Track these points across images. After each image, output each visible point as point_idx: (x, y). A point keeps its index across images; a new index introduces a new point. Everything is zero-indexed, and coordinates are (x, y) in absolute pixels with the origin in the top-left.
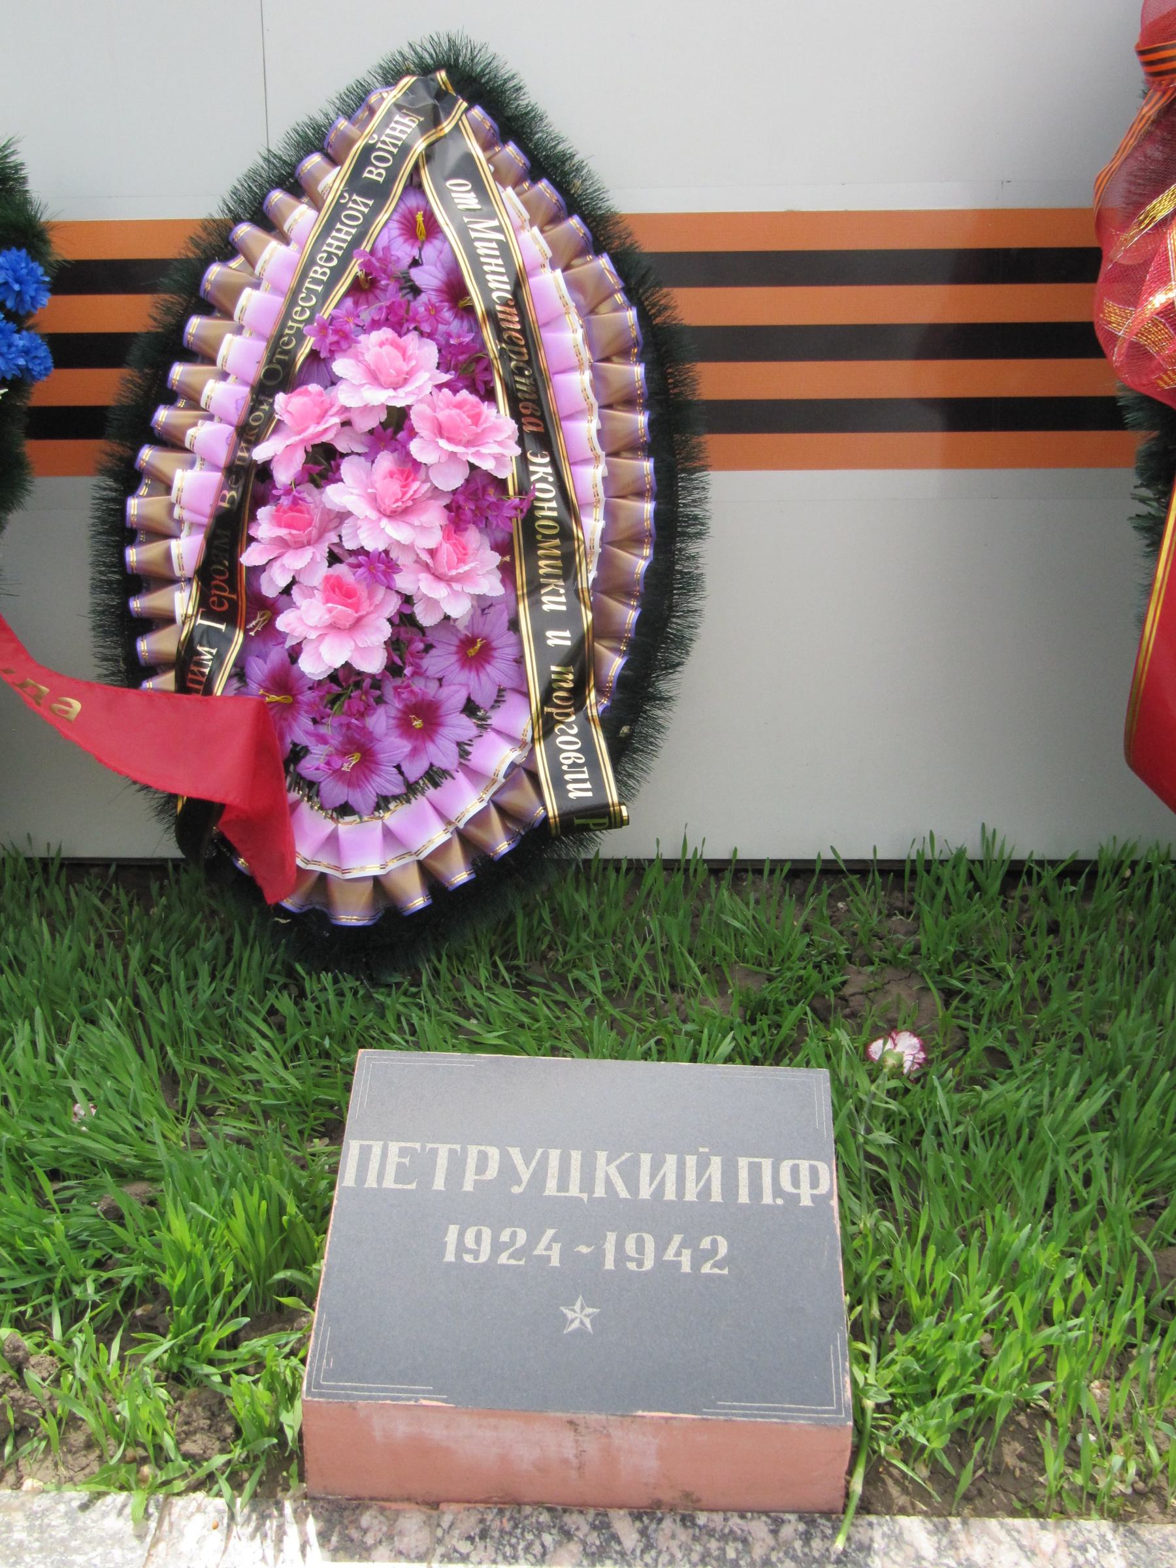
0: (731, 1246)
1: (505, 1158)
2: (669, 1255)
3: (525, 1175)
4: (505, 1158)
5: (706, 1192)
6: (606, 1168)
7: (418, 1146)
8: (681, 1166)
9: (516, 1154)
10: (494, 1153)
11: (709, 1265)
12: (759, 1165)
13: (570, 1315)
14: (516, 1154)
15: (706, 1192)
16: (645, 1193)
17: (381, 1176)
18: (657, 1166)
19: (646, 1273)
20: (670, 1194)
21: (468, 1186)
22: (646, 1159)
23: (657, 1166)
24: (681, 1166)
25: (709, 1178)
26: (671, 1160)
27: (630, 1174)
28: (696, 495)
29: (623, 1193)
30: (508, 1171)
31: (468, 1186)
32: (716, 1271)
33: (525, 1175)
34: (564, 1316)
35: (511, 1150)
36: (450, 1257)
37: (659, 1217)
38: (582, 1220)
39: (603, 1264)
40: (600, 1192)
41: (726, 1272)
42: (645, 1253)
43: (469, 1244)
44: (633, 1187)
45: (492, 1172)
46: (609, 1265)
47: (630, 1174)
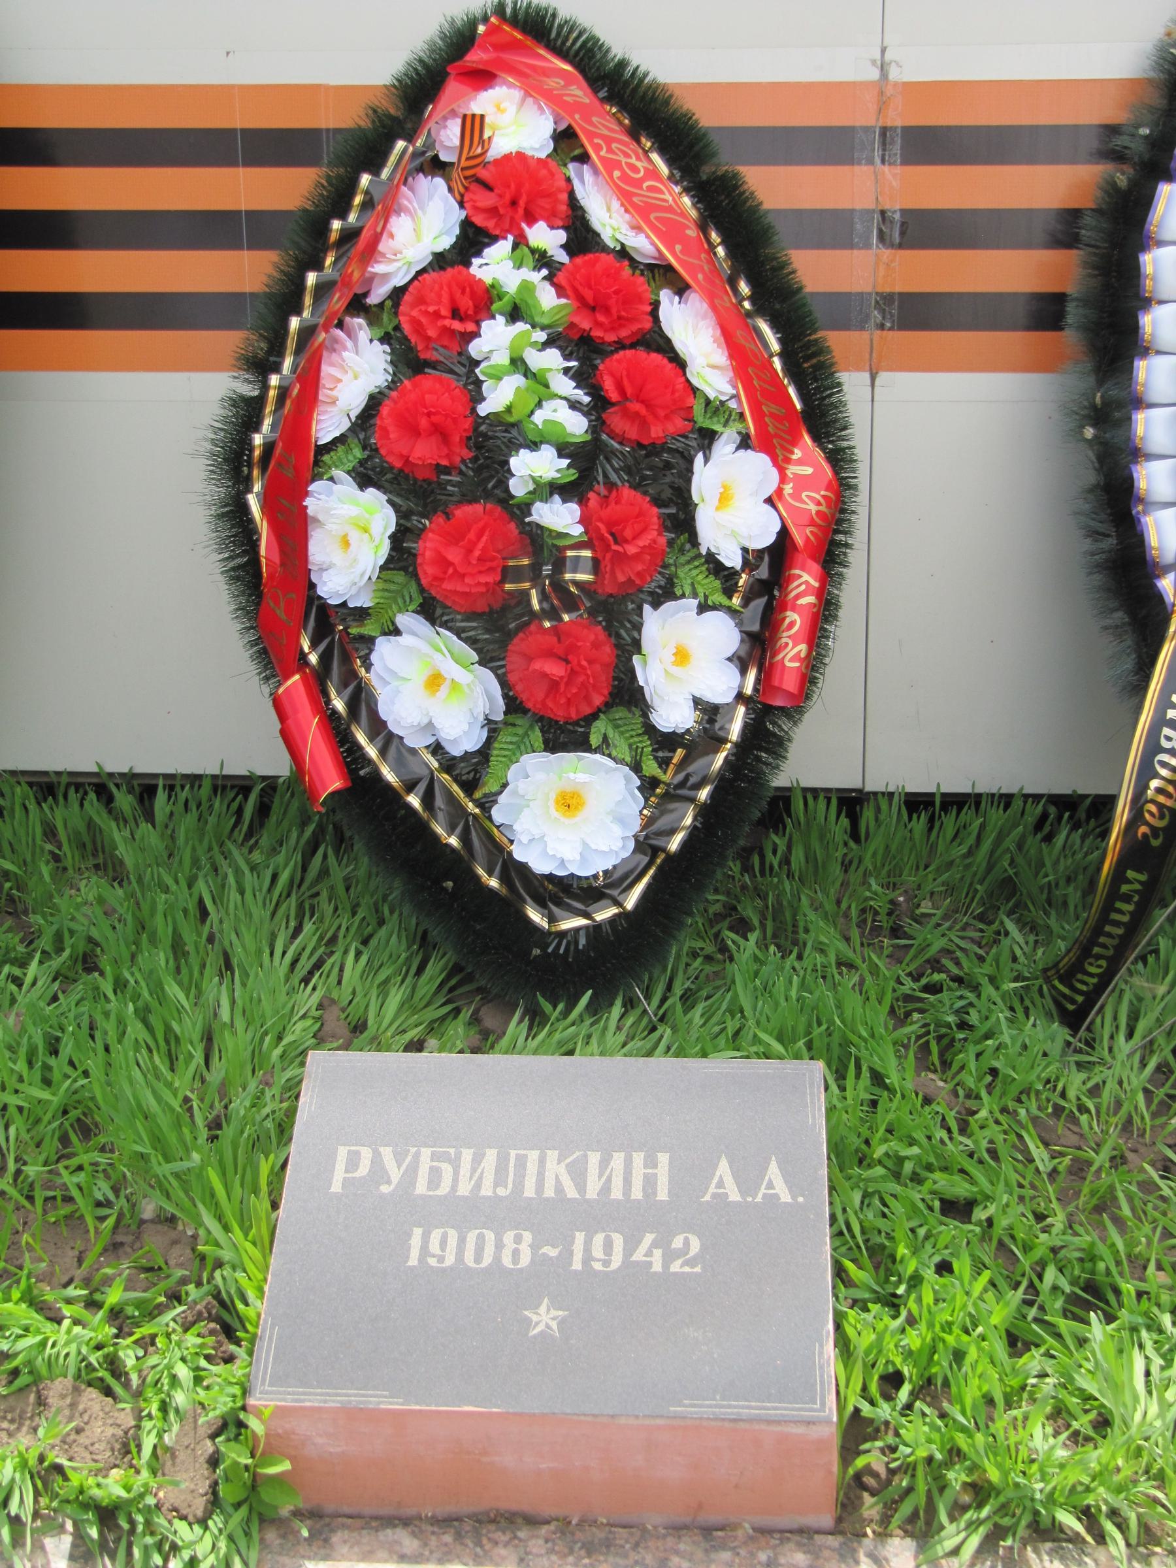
0: (704, 1248)
1: (377, 1159)
2: (639, 1256)
3: (395, 1174)
4: (377, 1159)
5: (606, 1189)
6: (556, 1168)
7: (452, 1151)
8: (628, 1163)
9: (387, 1153)
10: (366, 1153)
11: (680, 1261)
12: (358, 1153)
13: (543, 1309)
14: (387, 1153)
15: (606, 1189)
16: (592, 1191)
17: (454, 1187)
18: (604, 1163)
19: (521, 1270)
20: (617, 1193)
21: (336, 1187)
22: (594, 1158)
23: (604, 1163)
24: (628, 1163)
25: (481, 1178)
26: (618, 1159)
27: (579, 1174)
28: (550, 12)
29: (734, 1196)
30: (378, 1173)
31: (336, 1187)
32: (687, 1269)
33: (395, 1174)
34: (529, 1320)
35: (381, 1149)
36: (413, 1261)
37: (632, 1218)
38: (554, 1218)
39: (570, 1264)
40: (549, 1193)
41: (698, 1269)
42: (604, 1252)
43: (437, 1247)
44: (581, 1187)
45: (363, 1170)
46: (577, 1265)
47: (579, 1174)
